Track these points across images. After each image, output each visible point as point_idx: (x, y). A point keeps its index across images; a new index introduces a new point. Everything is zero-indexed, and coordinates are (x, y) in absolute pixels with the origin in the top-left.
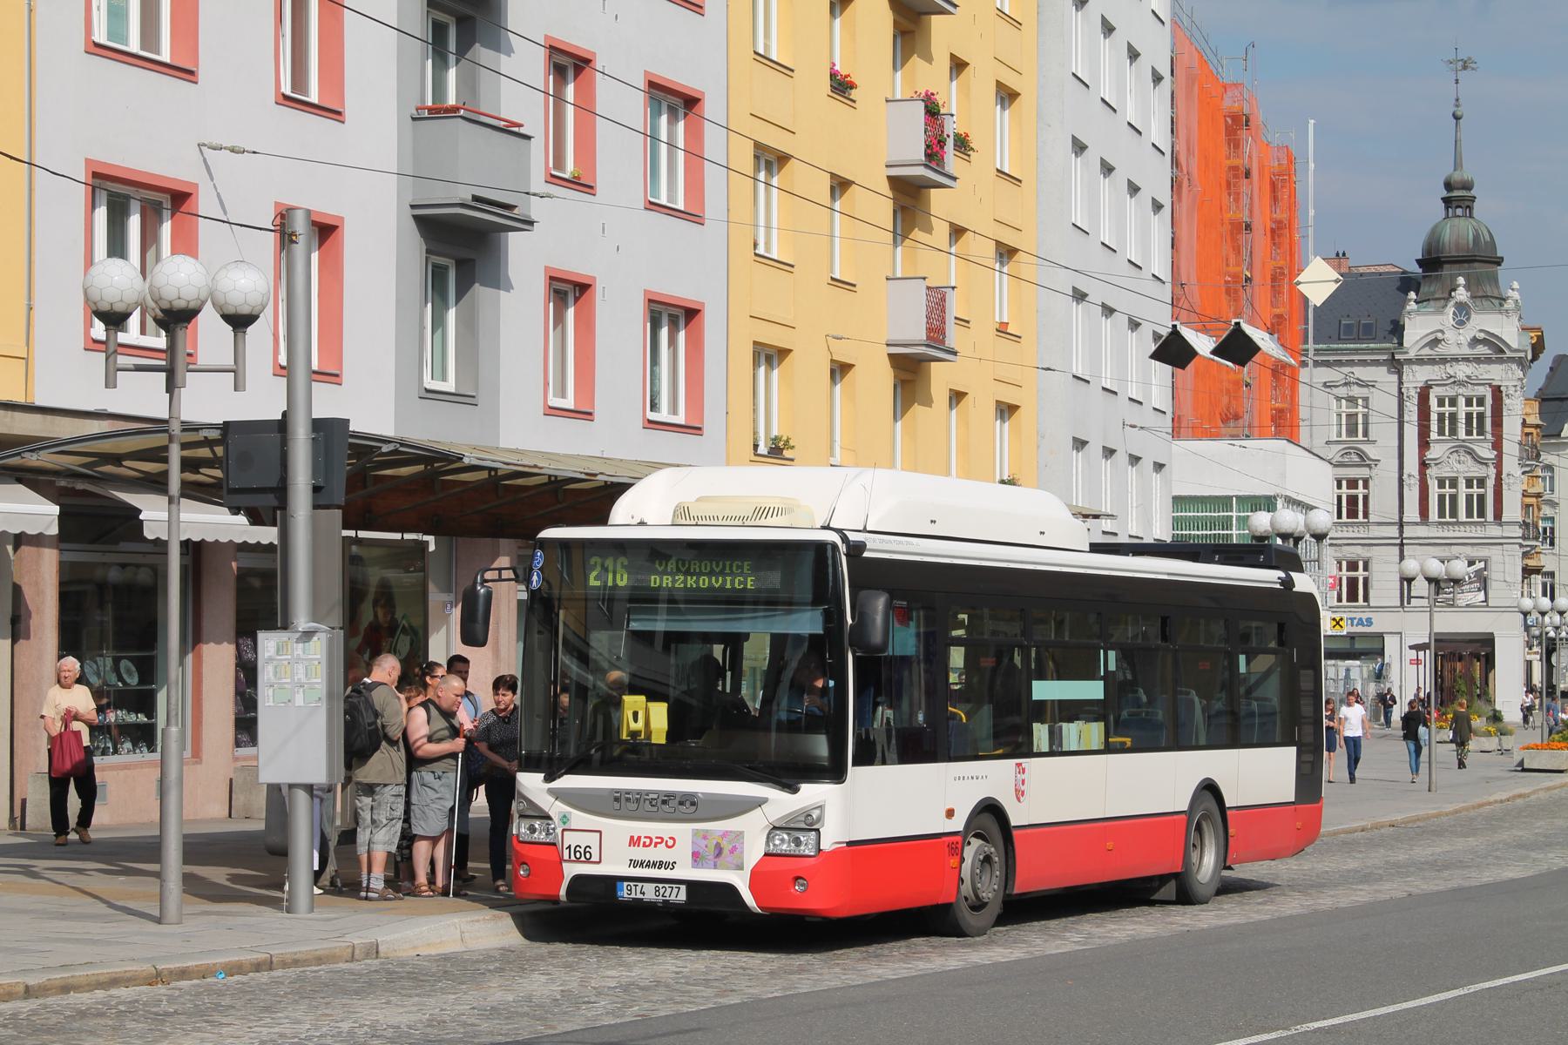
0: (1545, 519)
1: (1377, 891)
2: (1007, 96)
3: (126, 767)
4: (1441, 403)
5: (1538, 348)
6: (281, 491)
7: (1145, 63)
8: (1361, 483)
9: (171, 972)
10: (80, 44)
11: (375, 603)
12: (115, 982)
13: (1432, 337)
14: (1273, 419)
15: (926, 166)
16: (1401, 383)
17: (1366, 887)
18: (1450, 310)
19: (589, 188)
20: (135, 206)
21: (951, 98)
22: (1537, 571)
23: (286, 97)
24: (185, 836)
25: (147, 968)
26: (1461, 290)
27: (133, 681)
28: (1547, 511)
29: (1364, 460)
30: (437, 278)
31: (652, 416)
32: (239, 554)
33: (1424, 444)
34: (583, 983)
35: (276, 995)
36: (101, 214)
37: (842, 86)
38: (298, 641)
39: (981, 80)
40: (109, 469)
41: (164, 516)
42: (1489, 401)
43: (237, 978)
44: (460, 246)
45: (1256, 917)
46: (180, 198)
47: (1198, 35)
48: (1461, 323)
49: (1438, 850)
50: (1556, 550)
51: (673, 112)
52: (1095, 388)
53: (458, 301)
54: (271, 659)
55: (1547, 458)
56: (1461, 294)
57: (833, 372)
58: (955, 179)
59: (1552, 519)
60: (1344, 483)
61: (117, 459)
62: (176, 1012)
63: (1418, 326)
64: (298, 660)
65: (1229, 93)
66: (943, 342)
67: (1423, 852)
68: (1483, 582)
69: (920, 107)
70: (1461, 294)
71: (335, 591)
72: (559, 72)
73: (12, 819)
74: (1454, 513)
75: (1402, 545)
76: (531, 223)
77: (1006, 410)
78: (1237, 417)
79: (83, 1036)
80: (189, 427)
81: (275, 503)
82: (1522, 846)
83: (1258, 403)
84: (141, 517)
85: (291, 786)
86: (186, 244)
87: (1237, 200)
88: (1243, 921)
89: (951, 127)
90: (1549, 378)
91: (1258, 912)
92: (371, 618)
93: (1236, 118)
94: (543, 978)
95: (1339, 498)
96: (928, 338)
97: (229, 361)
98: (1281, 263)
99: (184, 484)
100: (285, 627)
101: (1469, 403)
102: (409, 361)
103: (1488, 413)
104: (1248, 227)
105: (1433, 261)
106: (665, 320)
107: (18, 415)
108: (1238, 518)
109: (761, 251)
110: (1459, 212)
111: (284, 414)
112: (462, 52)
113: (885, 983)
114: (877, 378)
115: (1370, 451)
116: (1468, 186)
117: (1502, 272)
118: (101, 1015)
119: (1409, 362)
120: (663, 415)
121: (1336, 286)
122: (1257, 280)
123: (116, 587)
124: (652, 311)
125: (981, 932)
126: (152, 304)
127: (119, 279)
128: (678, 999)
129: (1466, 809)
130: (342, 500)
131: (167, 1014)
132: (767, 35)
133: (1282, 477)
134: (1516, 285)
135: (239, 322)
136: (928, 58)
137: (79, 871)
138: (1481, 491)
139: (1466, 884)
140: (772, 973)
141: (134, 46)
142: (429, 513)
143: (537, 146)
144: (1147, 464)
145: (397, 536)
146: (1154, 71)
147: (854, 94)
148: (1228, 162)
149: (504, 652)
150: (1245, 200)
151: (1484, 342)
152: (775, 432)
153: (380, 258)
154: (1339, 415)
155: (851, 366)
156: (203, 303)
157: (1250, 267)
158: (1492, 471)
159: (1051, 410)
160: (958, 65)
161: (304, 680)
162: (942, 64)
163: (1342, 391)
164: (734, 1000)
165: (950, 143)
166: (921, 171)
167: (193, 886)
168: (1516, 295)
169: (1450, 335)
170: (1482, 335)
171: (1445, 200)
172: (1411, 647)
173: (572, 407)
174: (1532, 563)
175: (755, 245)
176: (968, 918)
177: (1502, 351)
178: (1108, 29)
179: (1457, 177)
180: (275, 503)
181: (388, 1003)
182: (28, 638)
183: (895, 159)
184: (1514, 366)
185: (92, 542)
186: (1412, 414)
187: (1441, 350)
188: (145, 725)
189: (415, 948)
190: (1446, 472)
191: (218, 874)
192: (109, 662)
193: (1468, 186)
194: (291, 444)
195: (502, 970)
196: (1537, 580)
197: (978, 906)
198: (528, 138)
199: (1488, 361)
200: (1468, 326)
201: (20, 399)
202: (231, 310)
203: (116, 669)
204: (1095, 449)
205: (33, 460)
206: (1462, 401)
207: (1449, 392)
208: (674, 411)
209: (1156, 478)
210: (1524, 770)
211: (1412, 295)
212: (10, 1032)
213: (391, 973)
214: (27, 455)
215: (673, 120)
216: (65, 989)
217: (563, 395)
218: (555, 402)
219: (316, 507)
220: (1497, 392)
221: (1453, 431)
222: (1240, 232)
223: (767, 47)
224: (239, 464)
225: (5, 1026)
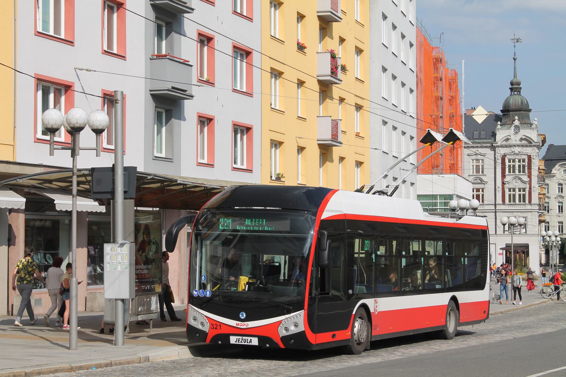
0: (546, 203)
1: (502, 337)
2: (359, 51)
4: (509, 161)
5: (544, 142)
6: (113, 193)
7: (407, 40)
8: (481, 190)
9: (76, 367)
10: (33, 32)
11: (143, 233)
13: (506, 138)
14: (450, 167)
15: (331, 76)
16: (495, 154)
17: (498, 335)
18: (513, 128)
19: (212, 84)
20: (52, 90)
21: (340, 52)
22: (544, 221)
23: (105, 51)
24: (79, 317)
25: (67, 366)
26: (516, 121)
28: (547, 200)
29: (482, 182)
30: (159, 116)
32: (89, 216)
33: (503, 176)
34: (225, 370)
36: (40, 93)
37: (301, 48)
38: (119, 247)
39: (350, 45)
41: (71, 202)
42: (527, 161)
43: (100, 369)
44: (167, 105)
45: (462, 346)
46: (68, 88)
48: (517, 133)
51: (242, 55)
52: (390, 156)
53: (166, 124)
55: (547, 181)
56: (517, 123)
57: (298, 150)
58: (341, 81)
59: (548, 203)
60: (475, 190)
61: (50, 181)
63: (501, 134)
64: (119, 254)
65: (434, 51)
66: (337, 139)
67: (516, 322)
68: (525, 226)
70: (517, 123)
71: (132, 228)
72: (202, 42)
73: (8, 312)
74: (514, 201)
75: (496, 212)
76: (192, 97)
77: (359, 164)
78: (437, 166)
80: (79, 170)
84: (55, 202)
85: (116, 300)
86: (70, 105)
87: (437, 89)
89: (340, 62)
90: (547, 152)
92: (142, 239)
93: (437, 59)
94: (210, 369)
95: (473, 195)
97: (95, 146)
98: (453, 111)
99: (78, 191)
101: (519, 161)
102: (149, 146)
103: (526, 165)
104: (441, 98)
105: (506, 111)
106: (239, 131)
107: (11, 166)
108: (440, 202)
109: (273, 106)
110: (516, 93)
111: (113, 165)
112: (167, 35)
114: (314, 152)
115: (484, 178)
116: (519, 84)
117: (531, 114)
119: (498, 146)
120: (239, 166)
121: (486, 116)
122: (444, 117)
123: (38, 228)
124: (234, 128)
125: (359, 353)
127: (54, 116)
130: (134, 197)
132: (275, 29)
133: (456, 186)
134: (536, 119)
135: (98, 132)
137: (41, 330)
138: (524, 193)
139: (533, 334)
140: (293, 367)
141: (52, 33)
142: (166, 201)
145: (151, 209)
147: (305, 50)
148: (434, 75)
150: (440, 89)
151: (525, 139)
152: (278, 172)
153: (138, 110)
154: (473, 166)
156: (86, 125)
157: (442, 113)
158: (528, 186)
160: (342, 40)
161: (121, 261)
162: (336, 39)
163: (474, 157)
165: (339, 68)
166: (329, 78)
168: (536, 123)
169: (513, 137)
170: (524, 137)
171: (511, 89)
172: (501, 249)
173: (63, 141)
174: (542, 218)
175: (271, 105)
176: (356, 348)
177: (531, 143)
178: (394, 27)
179: (515, 80)
180: (110, 197)
182: (14, 245)
183: (320, 74)
184: (536, 148)
185: (36, 211)
187: (510, 142)
189: (162, 358)
190: (511, 186)
191: (88, 331)
192: (42, 255)
193: (519, 84)
194: (116, 176)
195: (195, 366)
196: (543, 224)
197: (359, 344)
198: (191, 66)
199: (526, 146)
200: (519, 134)
201: (11, 160)
202: (95, 127)
203: (45, 257)
205: (20, 181)
207: (512, 157)
208: (242, 164)
209: (412, 188)
211: (499, 123)
213: (155, 367)
214: (18, 180)
215: (242, 61)
217: (203, 159)
219: (125, 198)
220: (529, 157)
221: (514, 172)
222: (438, 100)
223: (275, 33)
224: (97, 183)
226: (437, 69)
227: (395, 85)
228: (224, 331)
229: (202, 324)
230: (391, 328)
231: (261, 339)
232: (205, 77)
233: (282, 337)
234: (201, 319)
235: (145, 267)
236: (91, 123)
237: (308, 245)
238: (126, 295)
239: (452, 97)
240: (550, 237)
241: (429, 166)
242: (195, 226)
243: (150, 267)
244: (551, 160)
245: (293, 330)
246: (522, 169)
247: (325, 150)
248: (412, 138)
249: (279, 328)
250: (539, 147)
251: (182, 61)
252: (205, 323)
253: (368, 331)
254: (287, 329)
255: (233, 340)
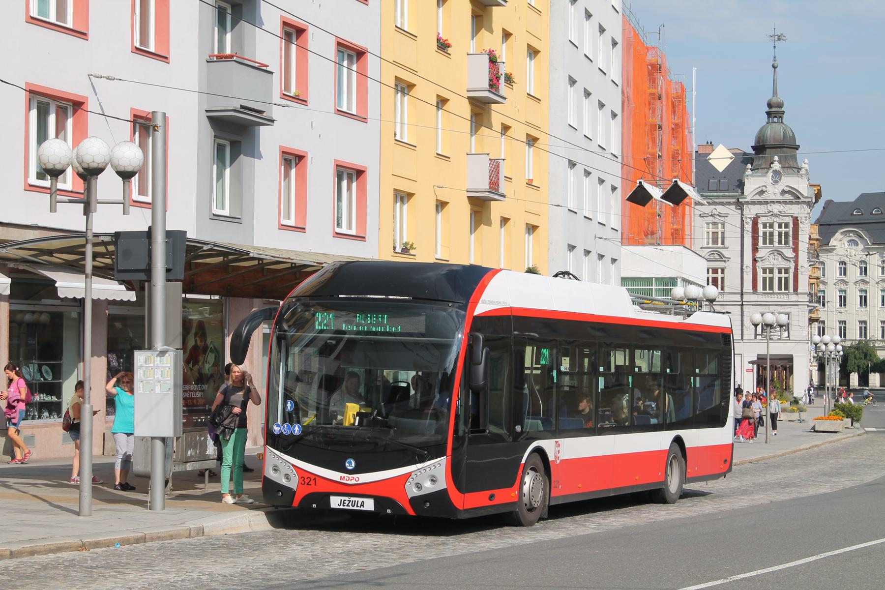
1: (752, 500)
2: (533, 52)
3: (46, 426)
5: (818, 196)
6: (148, 271)
8: (720, 271)
9: (90, 543)
12: (59, 549)
13: (760, 190)
14: (672, 234)
16: (742, 215)
17: (745, 497)
18: (770, 174)
19: (304, 102)
20: (53, 109)
21: (503, 53)
22: (817, 320)
23: (137, 49)
24: (94, 465)
25: (76, 541)
27: (50, 378)
28: (822, 287)
29: (721, 258)
31: (338, 230)
33: (755, 249)
34: (323, 550)
35: (152, 557)
36: (34, 113)
37: (443, 46)
38: (157, 356)
39: (519, 42)
40: (46, 258)
41: (83, 285)
42: (791, 225)
43: (126, 547)
44: (233, 134)
45: (689, 514)
46: (78, 105)
47: (633, 19)
48: (776, 182)
49: (780, 476)
50: (826, 309)
54: (141, 366)
55: (823, 257)
56: (776, 166)
57: (437, 206)
58: (505, 98)
59: (824, 291)
61: (50, 252)
62: (97, 566)
63: (753, 183)
64: (157, 367)
65: (650, 52)
66: (498, 190)
67: (773, 477)
69: (486, 58)
70: (776, 166)
71: (178, 329)
72: (288, 37)
74: (771, 288)
75: (742, 305)
76: (273, 121)
77: (532, 228)
78: (653, 233)
79: (48, 580)
80: (96, 235)
81: (145, 278)
82: (824, 474)
83: (663, 226)
85: (153, 438)
86: (81, 134)
87: (654, 112)
88: (683, 516)
89: (503, 70)
90: (822, 213)
91: (689, 511)
94: (300, 548)
95: (708, 279)
96: (490, 187)
97: (120, 198)
98: (678, 148)
100: (150, 348)
101: (780, 226)
102: (205, 196)
103: (791, 233)
104: (660, 127)
105: (760, 148)
106: (345, 176)
109: (398, 138)
110: (775, 120)
111: (150, 228)
112: (233, 26)
113: (493, 551)
114: (461, 210)
115: (725, 252)
116: (780, 105)
118: (56, 568)
119: (747, 203)
120: (344, 230)
121: (730, 161)
125: (530, 524)
126: (78, 165)
128: (379, 560)
129: (788, 453)
130: (182, 277)
131: (92, 567)
134: (806, 161)
135: (126, 175)
136: (491, 31)
139: (801, 496)
140: (427, 545)
141: (52, 19)
143: (276, 78)
144: (607, 259)
145: (207, 297)
146: (613, 39)
147: (450, 50)
149: (255, 363)
150: (658, 112)
151: (789, 192)
152: (405, 240)
153: (188, 140)
154: (708, 233)
155: (447, 203)
156: (107, 165)
157: (661, 150)
158: (793, 265)
159: (556, 228)
160: (507, 35)
161: (160, 378)
162: (498, 33)
163: (710, 219)
164: (410, 560)
165: (502, 80)
166: (486, 94)
167: (97, 494)
168: (806, 166)
169: (770, 188)
170: (787, 189)
172: (750, 363)
173: (70, 189)
174: (814, 316)
175: (395, 135)
177: (799, 198)
178: (588, 15)
179: (774, 100)
180: (145, 278)
181: (216, 561)
184: (805, 206)
185: (27, 299)
186: (748, 227)
187: (765, 197)
188: (57, 402)
189: (224, 530)
190: (767, 265)
192: (36, 366)
193: (780, 105)
195: (276, 543)
196: (816, 325)
197: (531, 509)
198: (272, 73)
199: (791, 203)
200: (780, 183)
202: (121, 169)
203: (40, 371)
204: (579, 251)
206: (776, 225)
208: (350, 228)
209: (613, 267)
210: (815, 431)
211: (749, 166)
212: (6, 578)
213: (213, 544)
215: (351, 62)
216: (32, 553)
217: (289, 218)
218: (285, 222)
219: (168, 280)
220: (796, 220)
221: (771, 242)
223: (402, 23)
224: (122, 255)
225: (2, 574)
226: (654, 82)
227: (589, 105)
228: (321, 488)
229: (287, 477)
230: (580, 485)
231: (378, 500)
232: (293, 91)
233: (412, 498)
234: (284, 469)
235: (198, 387)
236: (116, 162)
237: (452, 356)
238: (168, 430)
239: (677, 125)
240: (826, 344)
241: (639, 234)
242: (277, 324)
243: (205, 387)
244: (829, 225)
245: (429, 487)
246: (784, 238)
247: (479, 207)
248: (614, 189)
249: (407, 484)
250: (810, 205)
251: (257, 65)
252: (292, 476)
253: (544, 489)
254: (419, 486)
255: (335, 502)
